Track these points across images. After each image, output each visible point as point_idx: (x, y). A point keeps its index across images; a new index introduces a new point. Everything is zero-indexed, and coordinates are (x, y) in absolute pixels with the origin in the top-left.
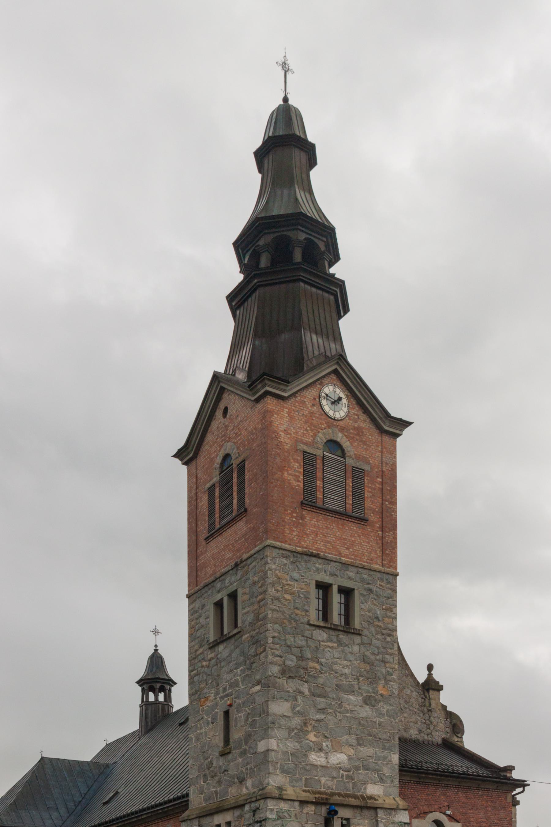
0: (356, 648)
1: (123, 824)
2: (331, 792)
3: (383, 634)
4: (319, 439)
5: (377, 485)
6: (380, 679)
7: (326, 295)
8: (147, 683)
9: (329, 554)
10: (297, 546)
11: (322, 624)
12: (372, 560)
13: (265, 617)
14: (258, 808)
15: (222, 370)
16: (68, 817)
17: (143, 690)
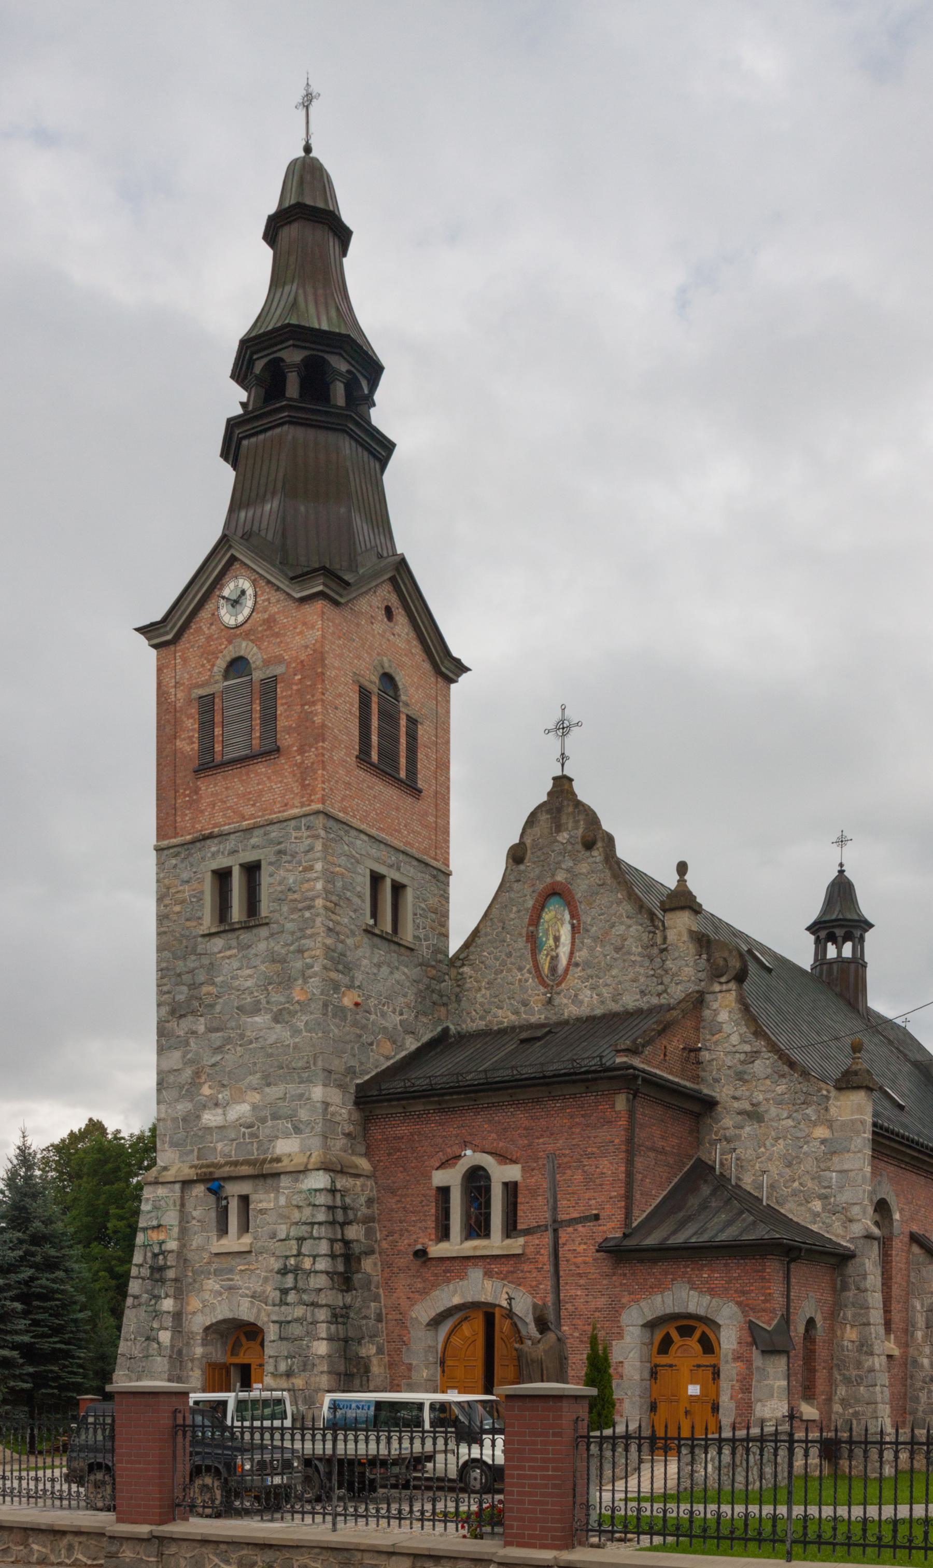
6: (295, 980)
8: (825, 928)
12: (286, 805)
17: (817, 941)
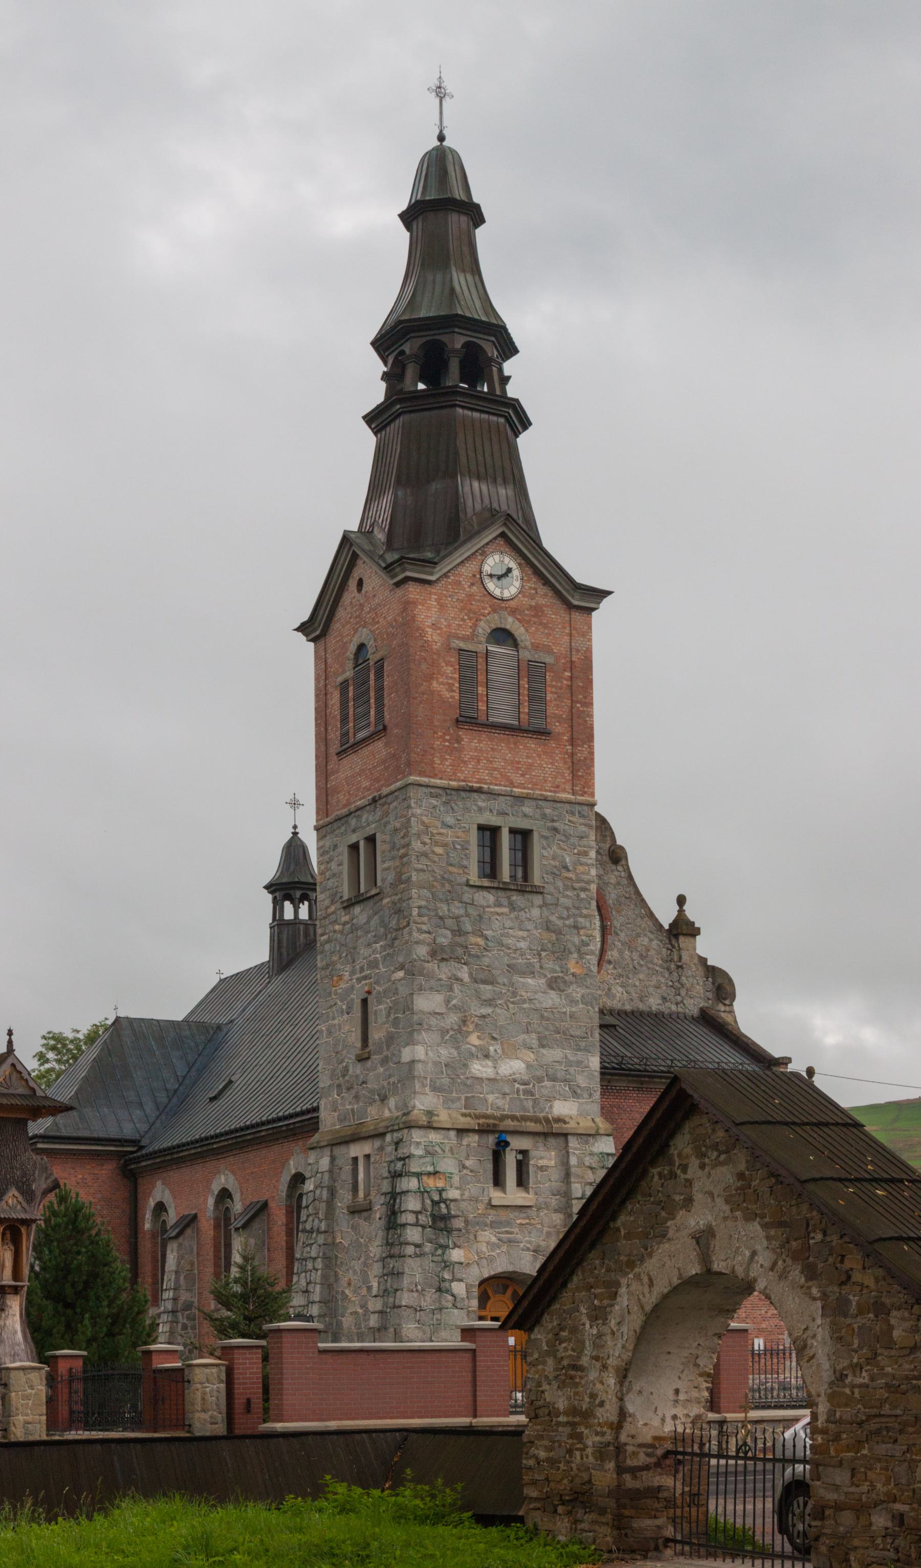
0: (536, 912)
1: (234, 1141)
3: (575, 889)
4: (480, 631)
5: (565, 682)
6: (570, 953)
8: (300, 888)
9: (496, 785)
10: (451, 780)
12: (557, 787)
13: (409, 880)
14: (401, 1140)
16: (157, 1118)
17: (275, 901)
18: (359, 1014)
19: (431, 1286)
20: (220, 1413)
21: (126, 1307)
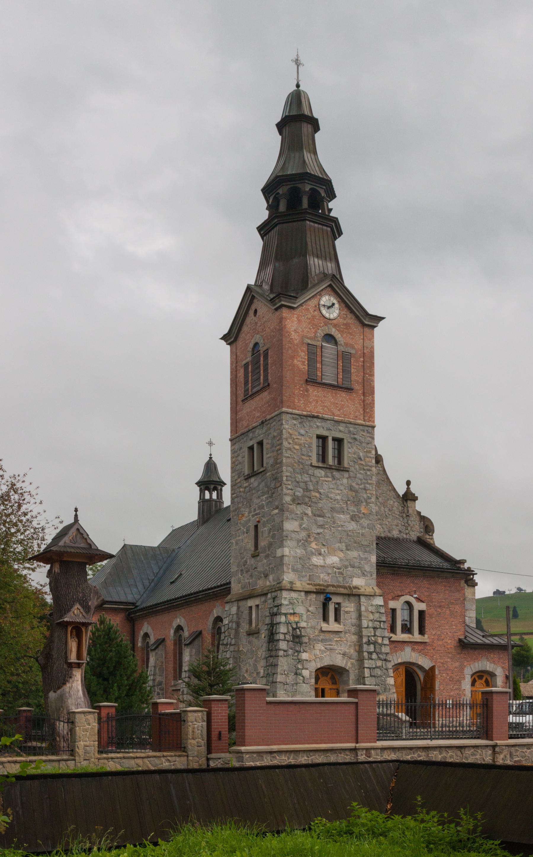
0: (345, 481)
2: (327, 585)
3: (364, 470)
4: (318, 334)
5: (361, 363)
6: (362, 502)
7: (325, 228)
8: (213, 484)
11: (321, 465)
12: (356, 417)
15: (252, 282)
16: (144, 592)
17: (201, 490)
18: (253, 533)
19: (292, 672)
20: (203, 740)
21: (136, 680)
